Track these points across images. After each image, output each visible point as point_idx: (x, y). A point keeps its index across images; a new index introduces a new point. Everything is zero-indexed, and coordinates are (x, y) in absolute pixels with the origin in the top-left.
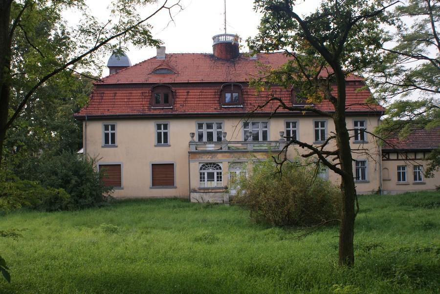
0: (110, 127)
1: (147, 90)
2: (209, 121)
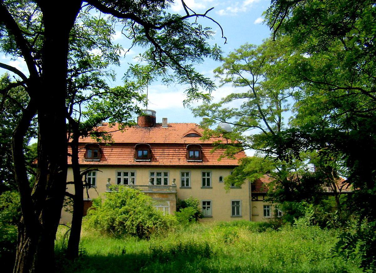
0: (206, 174)
2: (126, 170)
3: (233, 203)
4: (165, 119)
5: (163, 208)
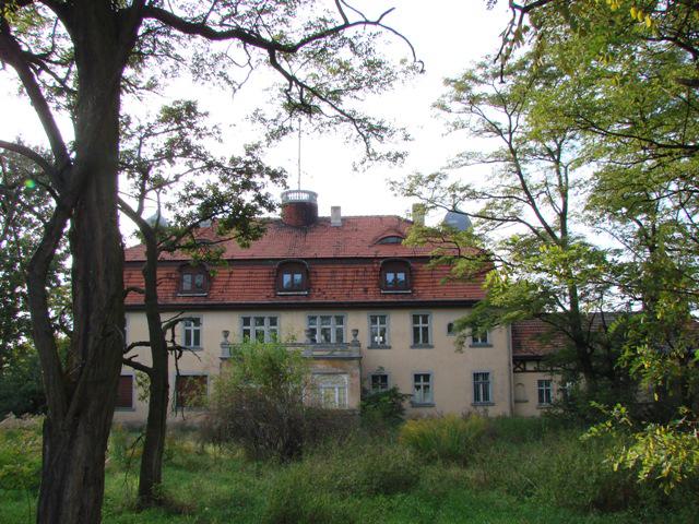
0: (421, 319)
1: (261, 273)
3: (476, 376)
4: (336, 209)
5: (333, 388)
